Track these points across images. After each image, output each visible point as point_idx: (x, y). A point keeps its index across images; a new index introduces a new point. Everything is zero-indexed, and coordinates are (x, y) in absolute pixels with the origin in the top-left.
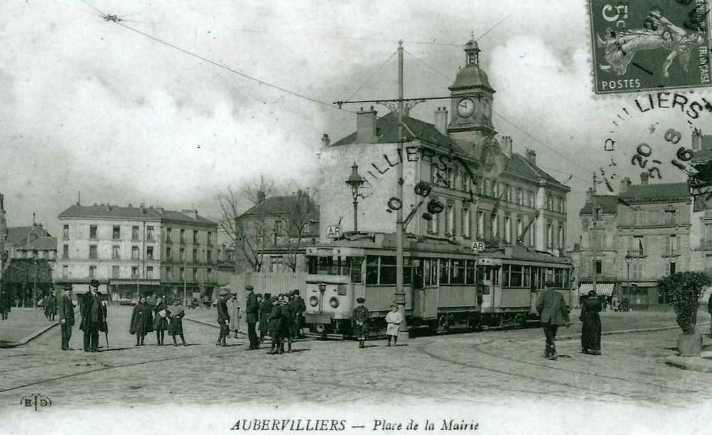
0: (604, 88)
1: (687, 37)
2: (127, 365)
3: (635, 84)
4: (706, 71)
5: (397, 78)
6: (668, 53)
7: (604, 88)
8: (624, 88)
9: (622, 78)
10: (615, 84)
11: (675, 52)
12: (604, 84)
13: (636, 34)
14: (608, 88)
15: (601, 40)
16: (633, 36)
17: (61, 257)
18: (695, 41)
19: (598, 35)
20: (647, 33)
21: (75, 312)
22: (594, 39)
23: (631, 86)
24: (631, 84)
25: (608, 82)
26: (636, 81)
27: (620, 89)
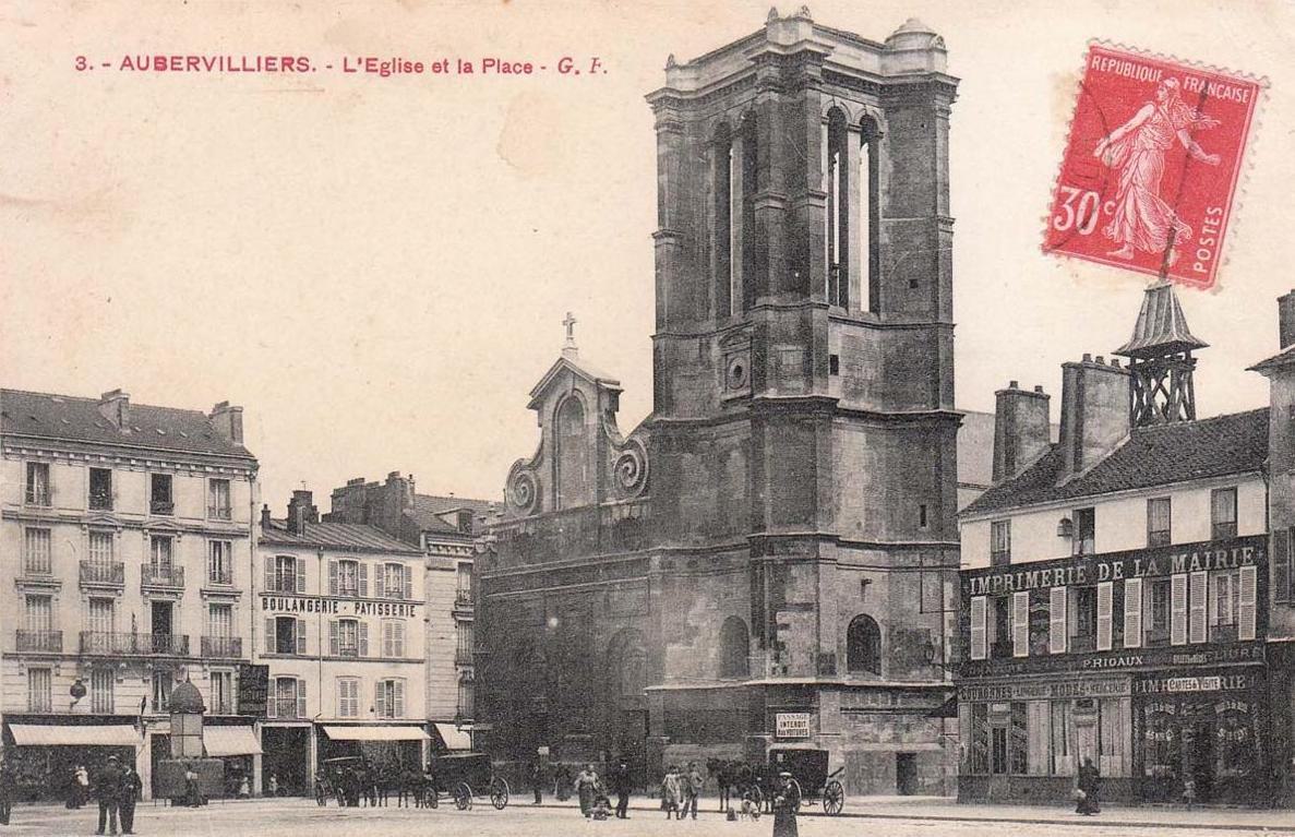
0: (1205, 271)
1: (1160, 103)
2: (1053, 753)
3: (1215, 217)
4: (1228, 88)
5: (1236, 831)
6: (1177, 142)
7: (1205, 271)
8: (1216, 237)
9: (1197, 234)
10: (1202, 259)
11: (1179, 133)
12: (1199, 268)
13: (1127, 190)
14: (1208, 265)
15: (1121, 251)
16: (1131, 194)
17: (734, 454)
18: (1171, 91)
19: (1109, 253)
20: (1131, 171)
21: (629, 806)
22: (1117, 262)
23: (1216, 224)
24: (1212, 222)
25: (1197, 260)
26: (1202, 243)
27: (1215, 245)
